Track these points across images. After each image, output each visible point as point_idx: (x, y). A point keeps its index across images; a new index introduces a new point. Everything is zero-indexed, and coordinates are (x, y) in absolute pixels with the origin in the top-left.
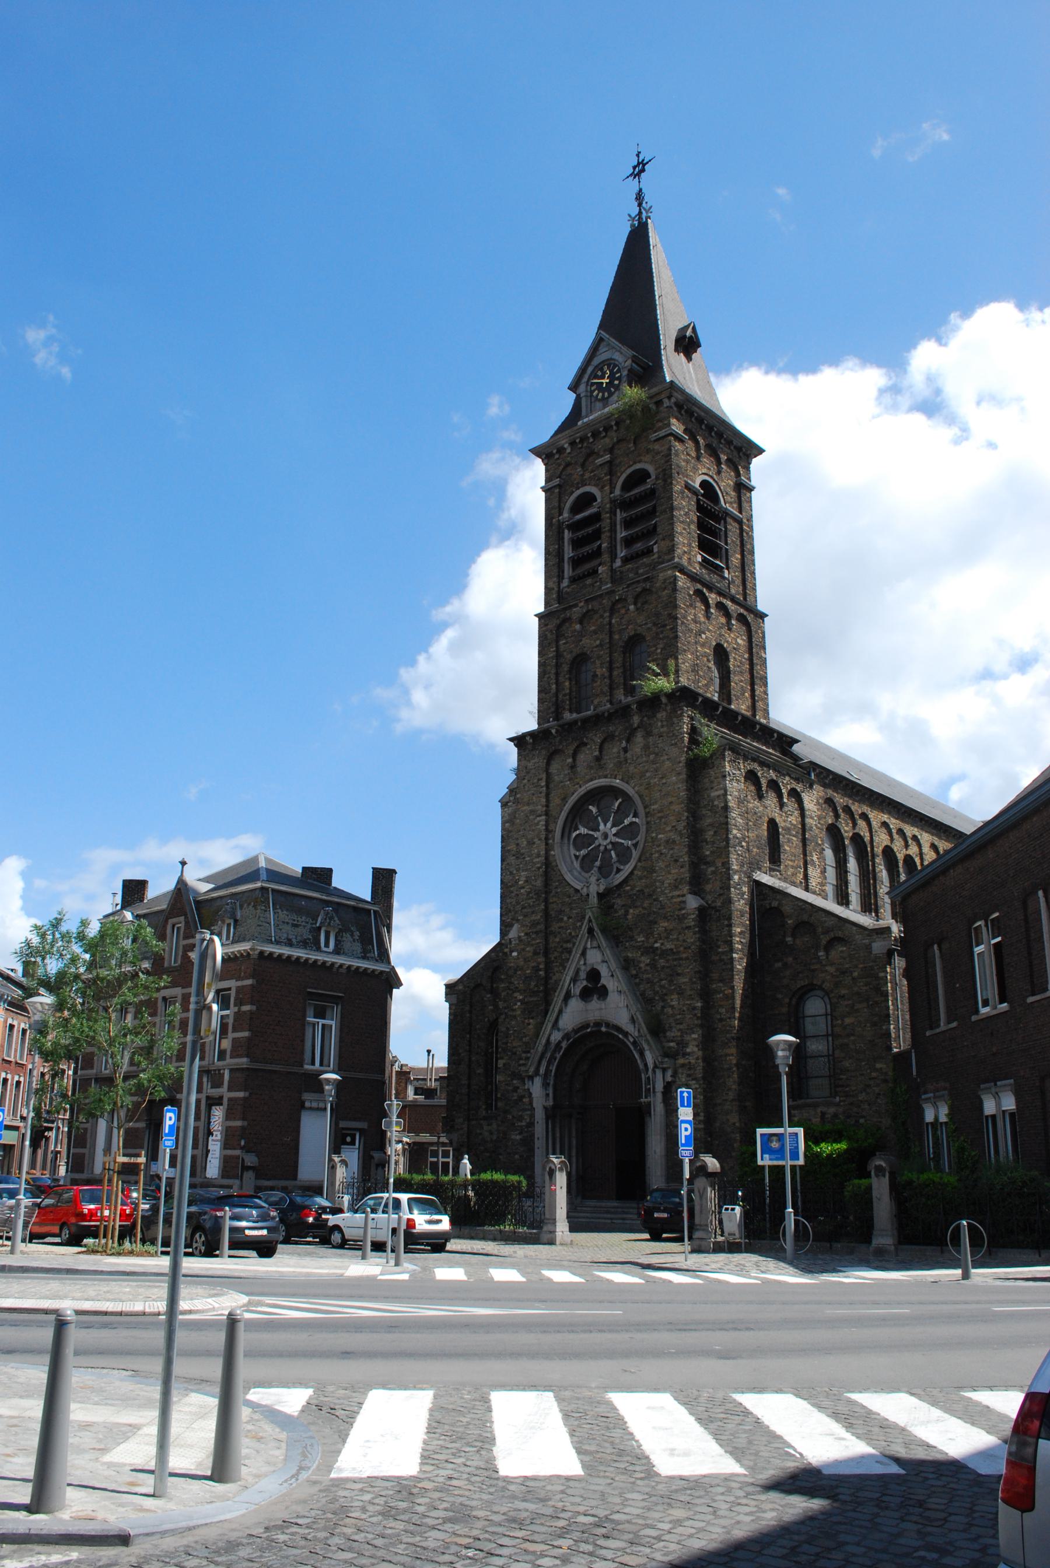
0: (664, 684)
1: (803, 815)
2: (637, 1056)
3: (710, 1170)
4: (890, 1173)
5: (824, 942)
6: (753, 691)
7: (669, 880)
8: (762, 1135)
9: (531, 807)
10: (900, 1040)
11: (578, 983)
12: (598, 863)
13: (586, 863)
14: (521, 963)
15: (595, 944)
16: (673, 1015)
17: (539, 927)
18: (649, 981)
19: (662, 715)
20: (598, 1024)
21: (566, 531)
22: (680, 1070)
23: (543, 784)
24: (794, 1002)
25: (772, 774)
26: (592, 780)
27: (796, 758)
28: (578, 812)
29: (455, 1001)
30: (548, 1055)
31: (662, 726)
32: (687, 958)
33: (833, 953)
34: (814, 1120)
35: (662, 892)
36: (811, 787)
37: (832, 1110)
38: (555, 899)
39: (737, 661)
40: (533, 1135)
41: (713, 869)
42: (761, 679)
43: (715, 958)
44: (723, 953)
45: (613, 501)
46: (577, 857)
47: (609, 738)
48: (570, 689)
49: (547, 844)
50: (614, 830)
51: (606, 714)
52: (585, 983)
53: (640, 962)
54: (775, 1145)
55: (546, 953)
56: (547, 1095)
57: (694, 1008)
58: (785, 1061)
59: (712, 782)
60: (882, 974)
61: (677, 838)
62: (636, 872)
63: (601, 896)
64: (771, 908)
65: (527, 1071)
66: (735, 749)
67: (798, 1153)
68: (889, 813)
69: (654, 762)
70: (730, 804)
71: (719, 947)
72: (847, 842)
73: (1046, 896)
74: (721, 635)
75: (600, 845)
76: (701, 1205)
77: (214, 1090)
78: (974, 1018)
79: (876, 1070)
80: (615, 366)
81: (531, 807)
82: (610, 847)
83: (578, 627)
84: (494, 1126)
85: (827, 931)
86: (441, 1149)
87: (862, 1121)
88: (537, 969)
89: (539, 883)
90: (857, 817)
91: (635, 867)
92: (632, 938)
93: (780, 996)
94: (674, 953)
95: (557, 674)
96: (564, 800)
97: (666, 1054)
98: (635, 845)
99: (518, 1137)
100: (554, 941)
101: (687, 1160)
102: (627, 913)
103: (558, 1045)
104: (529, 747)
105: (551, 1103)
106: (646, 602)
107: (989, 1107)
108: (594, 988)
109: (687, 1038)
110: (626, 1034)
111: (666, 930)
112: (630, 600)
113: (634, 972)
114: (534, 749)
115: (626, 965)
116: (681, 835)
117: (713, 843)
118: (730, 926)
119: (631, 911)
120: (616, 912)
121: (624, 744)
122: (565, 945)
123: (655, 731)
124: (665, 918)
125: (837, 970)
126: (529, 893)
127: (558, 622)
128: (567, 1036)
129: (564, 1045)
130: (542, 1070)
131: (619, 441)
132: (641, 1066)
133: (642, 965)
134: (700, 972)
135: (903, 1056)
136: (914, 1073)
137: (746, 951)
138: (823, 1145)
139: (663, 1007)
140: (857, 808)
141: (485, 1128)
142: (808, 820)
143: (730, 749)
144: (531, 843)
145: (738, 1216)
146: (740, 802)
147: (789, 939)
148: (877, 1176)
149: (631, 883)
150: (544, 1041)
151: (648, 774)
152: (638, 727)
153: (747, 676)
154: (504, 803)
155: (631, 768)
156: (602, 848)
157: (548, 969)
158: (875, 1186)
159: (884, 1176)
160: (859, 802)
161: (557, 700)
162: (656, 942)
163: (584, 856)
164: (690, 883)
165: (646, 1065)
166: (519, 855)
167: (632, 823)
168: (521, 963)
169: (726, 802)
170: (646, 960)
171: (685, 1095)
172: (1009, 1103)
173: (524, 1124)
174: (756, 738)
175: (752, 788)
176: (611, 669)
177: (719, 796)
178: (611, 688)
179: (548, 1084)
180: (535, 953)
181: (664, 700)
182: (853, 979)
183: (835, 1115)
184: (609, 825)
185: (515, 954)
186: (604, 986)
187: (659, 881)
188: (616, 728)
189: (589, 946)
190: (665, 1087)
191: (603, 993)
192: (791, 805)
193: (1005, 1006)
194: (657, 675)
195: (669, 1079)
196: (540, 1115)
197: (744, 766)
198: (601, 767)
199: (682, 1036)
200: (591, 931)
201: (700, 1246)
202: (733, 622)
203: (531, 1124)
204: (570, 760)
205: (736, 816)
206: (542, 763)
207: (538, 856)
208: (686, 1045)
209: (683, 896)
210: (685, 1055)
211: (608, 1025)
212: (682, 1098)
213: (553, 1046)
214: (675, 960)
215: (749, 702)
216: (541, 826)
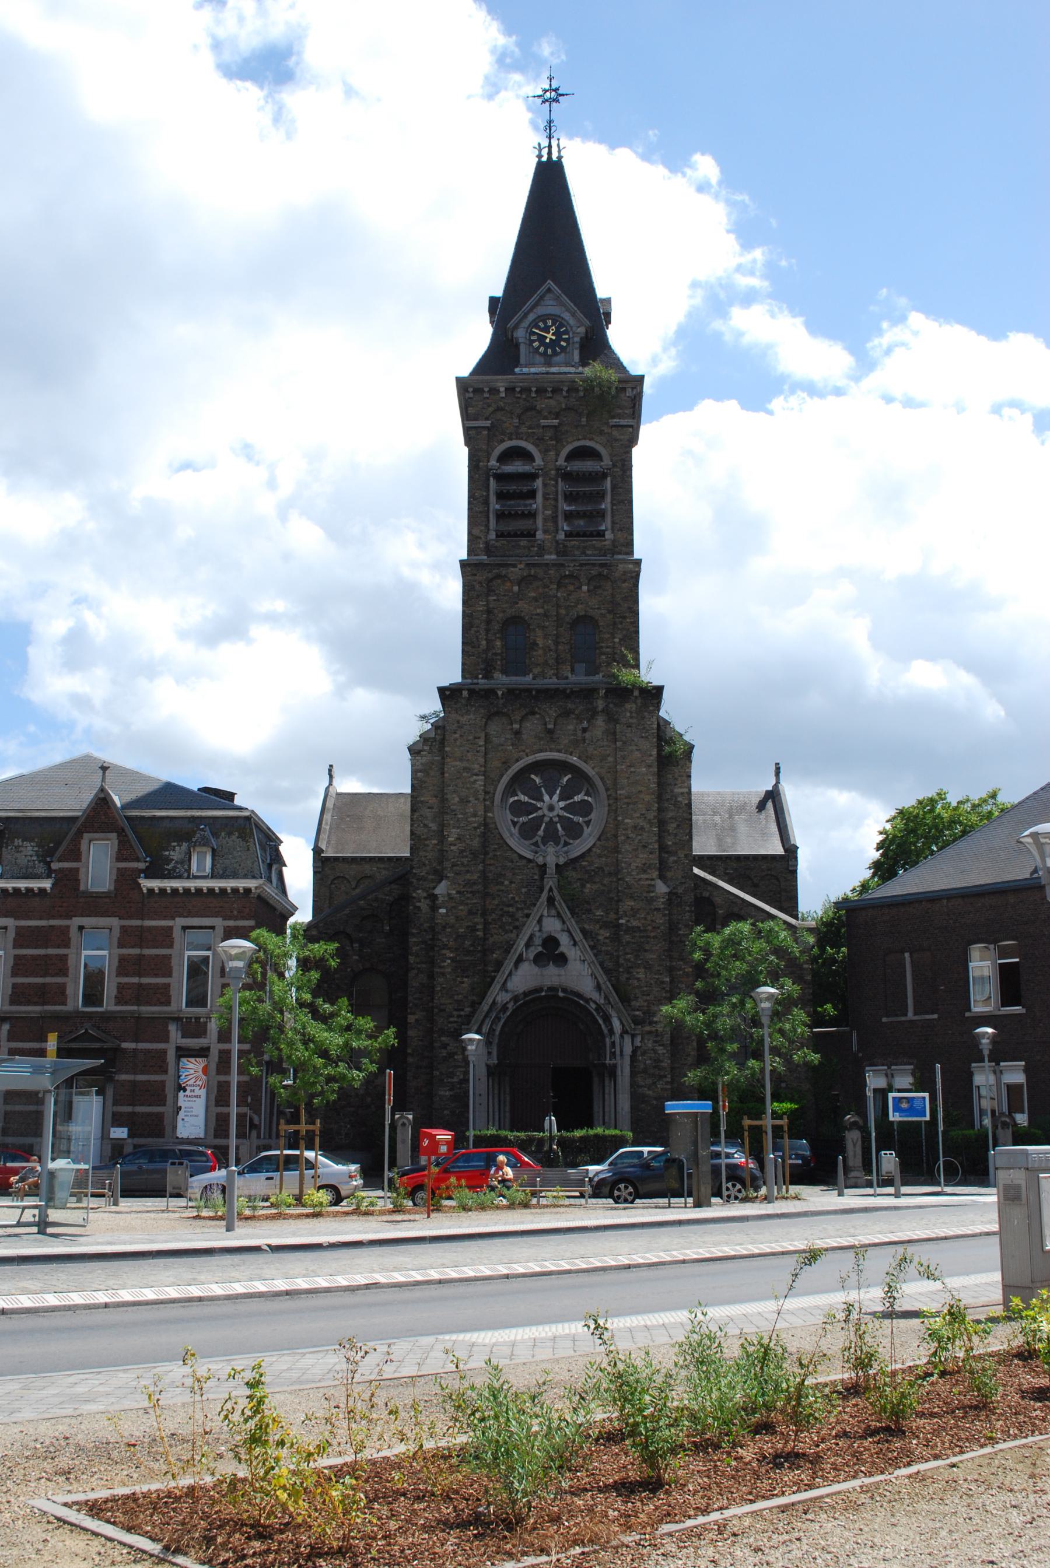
9: (465, 764)
11: (532, 948)
14: (452, 920)
16: (639, 987)
17: (475, 888)
18: (607, 953)
20: (551, 989)
21: (491, 479)
23: (482, 743)
26: (542, 751)
28: (520, 780)
31: (631, 717)
32: (655, 937)
35: (629, 874)
38: (492, 862)
44: (684, 935)
45: (558, 469)
47: (566, 713)
50: (562, 804)
51: (568, 691)
52: (540, 949)
53: (597, 934)
54: (904, 1105)
55: (484, 914)
56: (489, 1053)
57: (663, 982)
61: (647, 826)
62: (594, 850)
71: (680, 929)
75: (544, 816)
77: (184, 1041)
78: (967, 1014)
83: (516, 588)
88: (473, 929)
89: (476, 843)
92: (589, 911)
94: (641, 931)
96: (506, 764)
97: (636, 1022)
102: (583, 886)
103: (504, 1008)
106: (600, 587)
108: (550, 953)
111: (632, 909)
116: (650, 822)
117: (676, 835)
119: (588, 885)
122: (506, 909)
123: (624, 720)
124: (631, 897)
126: (462, 851)
127: (490, 575)
128: (515, 999)
129: (510, 1006)
131: (568, 409)
132: (606, 1031)
136: (855, 1048)
144: (464, 801)
155: (590, 749)
156: (546, 819)
173: (455, 1080)
177: (682, 793)
179: (491, 1043)
180: (471, 913)
181: (636, 693)
187: (626, 863)
199: (648, 1006)
200: (551, 901)
207: (475, 815)
209: (652, 880)
210: (651, 1023)
211: (564, 990)
213: (499, 1006)
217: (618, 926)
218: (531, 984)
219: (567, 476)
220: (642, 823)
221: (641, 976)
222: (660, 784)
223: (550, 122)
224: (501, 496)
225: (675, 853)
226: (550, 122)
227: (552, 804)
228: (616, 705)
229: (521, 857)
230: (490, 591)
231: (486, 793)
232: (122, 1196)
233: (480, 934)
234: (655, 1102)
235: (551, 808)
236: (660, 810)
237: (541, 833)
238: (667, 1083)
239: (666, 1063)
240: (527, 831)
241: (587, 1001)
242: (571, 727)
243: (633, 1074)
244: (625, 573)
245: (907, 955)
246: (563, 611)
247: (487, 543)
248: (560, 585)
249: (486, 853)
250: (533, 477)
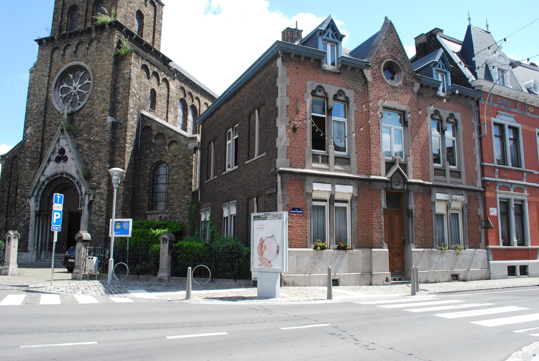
0: (107, 19)
1: (169, 91)
2: (78, 189)
3: (84, 239)
4: (169, 241)
5: (168, 142)
6: (154, 36)
9: (42, 73)
10: (195, 184)
12: (70, 101)
13: (65, 100)
14: (31, 144)
15: (64, 137)
16: (96, 170)
18: (87, 155)
19: (105, 34)
20: (62, 174)
22: (97, 196)
23: (49, 62)
24: (153, 168)
25: (156, 69)
26: (71, 62)
27: (169, 67)
28: (64, 77)
29: (4, 163)
30: (38, 187)
32: (105, 145)
33: (172, 147)
34: (157, 220)
35: (97, 115)
36: (174, 79)
37: (165, 215)
39: (148, 20)
40: (29, 224)
41: (121, 105)
42: (158, 31)
43: (118, 146)
46: (61, 97)
47: (81, 43)
48: (68, 21)
49: (48, 90)
50: (79, 86)
52: (58, 154)
53: (84, 146)
55: (42, 140)
56: (37, 205)
57: (106, 168)
58: (116, 182)
59: (125, 66)
60: (191, 157)
61: (106, 90)
63: (69, 115)
64: (147, 127)
65: (28, 194)
66: (136, 53)
67: (128, 231)
68: (209, 100)
69: (99, 55)
70: (132, 77)
72: (189, 107)
73: (259, 113)
74: (141, 7)
76: (79, 256)
78: (224, 173)
79: (185, 199)
81: (42, 73)
82: (76, 93)
87: (177, 220)
88: (37, 148)
89: (42, 108)
90: (194, 98)
91: (86, 103)
92: (81, 135)
93: (147, 165)
95: (62, 13)
96: (58, 70)
98: (87, 93)
99: (23, 225)
100: (47, 135)
101: (56, 232)
102: (80, 123)
103: (43, 183)
104: (44, 45)
105: (38, 209)
107: (226, 214)
108: (62, 157)
109: (101, 181)
110: (74, 178)
113: (81, 151)
114: (46, 46)
115: (78, 147)
116: (108, 89)
117: (123, 94)
118: (126, 131)
120: (76, 123)
121: (87, 46)
123: (102, 41)
124: (97, 126)
125: (173, 155)
128: (47, 179)
129: (46, 183)
130: (35, 194)
132: (80, 193)
133: (85, 147)
134: (110, 151)
135: (196, 192)
137: (133, 144)
138: (157, 230)
139: (92, 167)
140: (195, 94)
141: (14, 221)
142: (170, 93)
143: (135, 52)
144: (40, 89)
145: (95, 262)
146: (137, 77)
147: (153, 140)
148: (163, 242)
149: (84, 110)
150: (37, 181)
151: (96, 61)
152: (95, 39)
153: (152, 28)
155: (89, 57)
156: (73, 94)
157: (42, 148)
158: (162, 247)
159: (166, 243)
160: (196, 92)
161: (61, 25)
162: (92, 137)
163: (65, 97)
164: (110, 111)
165: (82, 193)
166: (34, 95)
167: (88, 83)
168: (31, 144)
169: (130, 75)
170: (87, 145)
171: (59, 197)
172: (234, 211)
174: (151, 54)
175: (145, 73)
176: (86, 13)
178: (86, 21)
180: (37, 140)
181: (107, 26)
182: (179, 159)
183: (166, 218)
184: (77, 83)
185: (28, 140)
186: (66, 156)
188: (85, 38)
189: (61, 137)
190: (89, 203)
191: (66, 159)
192: (163, 85)
193: (236, 167)
194: (105, 14)
195: (91, 199)
196: (33, 214)
197: (142, 62)
198: (76, 56)
200: (62, 131)
201: (76, 276)
202: (148, 3)
203: (29, 219)
204: (62, 52)
205: (134, 83)
207: (43, 95)
209: (106, 116)
210: (99, 188)
211: (66, 174)
212: (56, 198)
213: (41, 183)
214: (99, 145)
215: (152, 40)
216: (46, 82)
221: (97, 165)
228: (100, 34)
232: (333, 285)
234: (98, 229)
239: (104, 209)
243: (90, 214)
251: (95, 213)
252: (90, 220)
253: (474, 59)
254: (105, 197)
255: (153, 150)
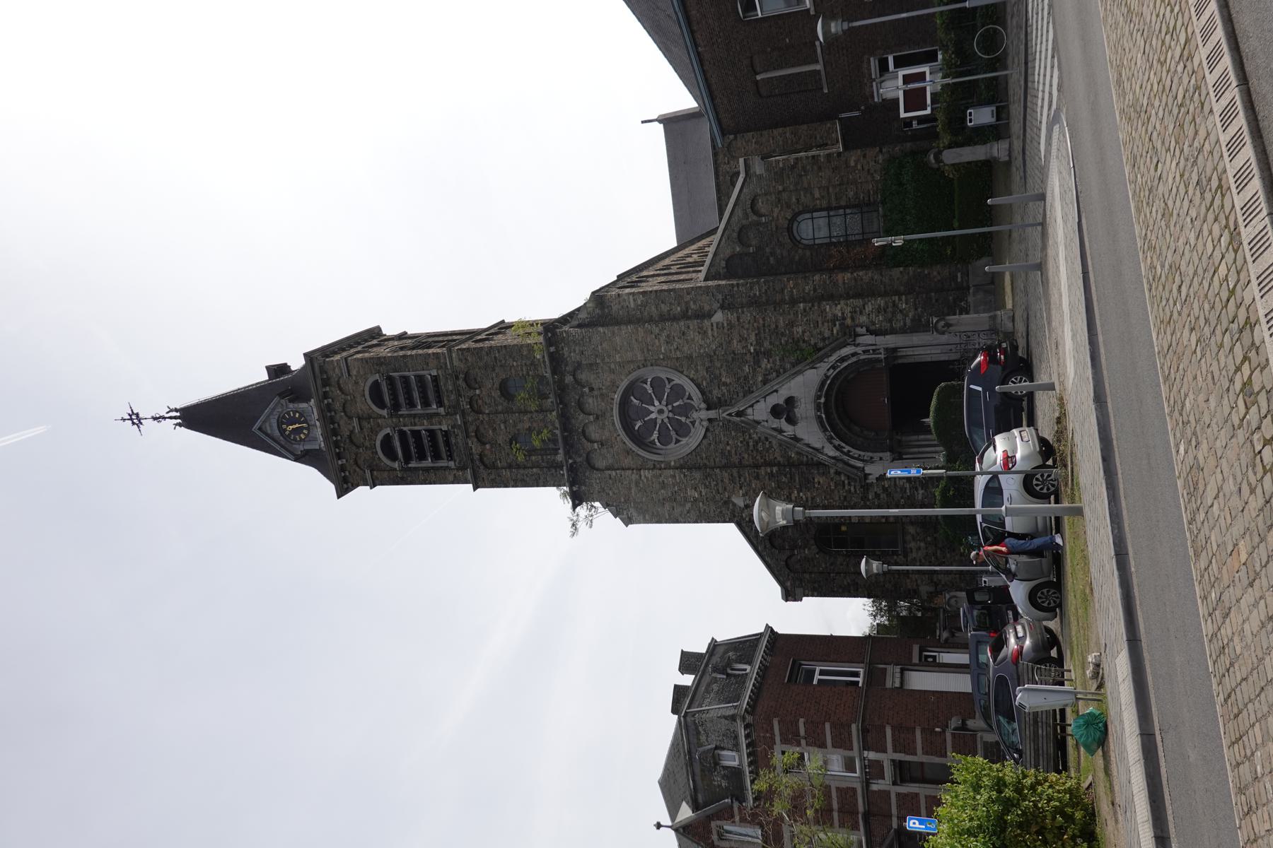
2: (845, 364)
5: (755, 218)
7: (698, 338)
8: (906, 111)
9: (633, 485)
17: (735, 474)
18: (782, 360)
20: (818, 408)
23: (614, 473)
28: (639, 439)
30: (846, 458)
33: (763, 211)
45: (391, 416)
47: (580, 406)
55: (757, 466)
61: (664, 334)
78: (812, 12)
80: (284, 417)
83: (488, 446)
84: (913, 545)
85: (746, 216)
86: (928, 111)
88: (771, 475)
89: (697, 475)
92: (746, 378)
96: (628, 452)
99: (921, 492)
102: (725, 384)
108: (785, 411)
112: (471, 393)
116: (662, 330)
120: (723, 395)
123: (578, 358)
126: (706, 487)
128: (830, 440)
129: (837, 442)
130: (860, 464)
132: (854, 359)
136: (857, 114)
141: (914, 555)
144: (663, 485)
154: (628, 521)
156: (671, 415)
180: (757, 477)
184: (652, 408)
191: (790, 401)
206: (596, 475)
207: (674, 476)
208: (835, 316)
211: (819, 397)
213: (837, 454)
217: (757, 353)
218: (815, 427)
219: (396, 406)
220: (663, 338)
221: (800, 330)
222: (630, 322)
223: (155, 419)
224: (422, 457)
225: (687, 303)
226: (155, 419)
227: (657, 411)
229: (705, 437)
230: (494, 467)
231: (654, 467)
233: (775, 469)
235: (660, 412)
236: (651, 320)
237: (683, 419)
238: (900, 299)
239: (881, 301)
240: (683, 430)
241: (827, 377)
242: (590, 400)
243: (893, 331)
244: (460, 360)
245: (758, 78)
246: (500, 408)
247: (458, 469)
248: (479, 412)
249: (705, 466)
250: (402, 435)
251: (890, 321)
252: (903, 331)
253: (297, 363)
254: (858, 302)
255: (768, 250)
